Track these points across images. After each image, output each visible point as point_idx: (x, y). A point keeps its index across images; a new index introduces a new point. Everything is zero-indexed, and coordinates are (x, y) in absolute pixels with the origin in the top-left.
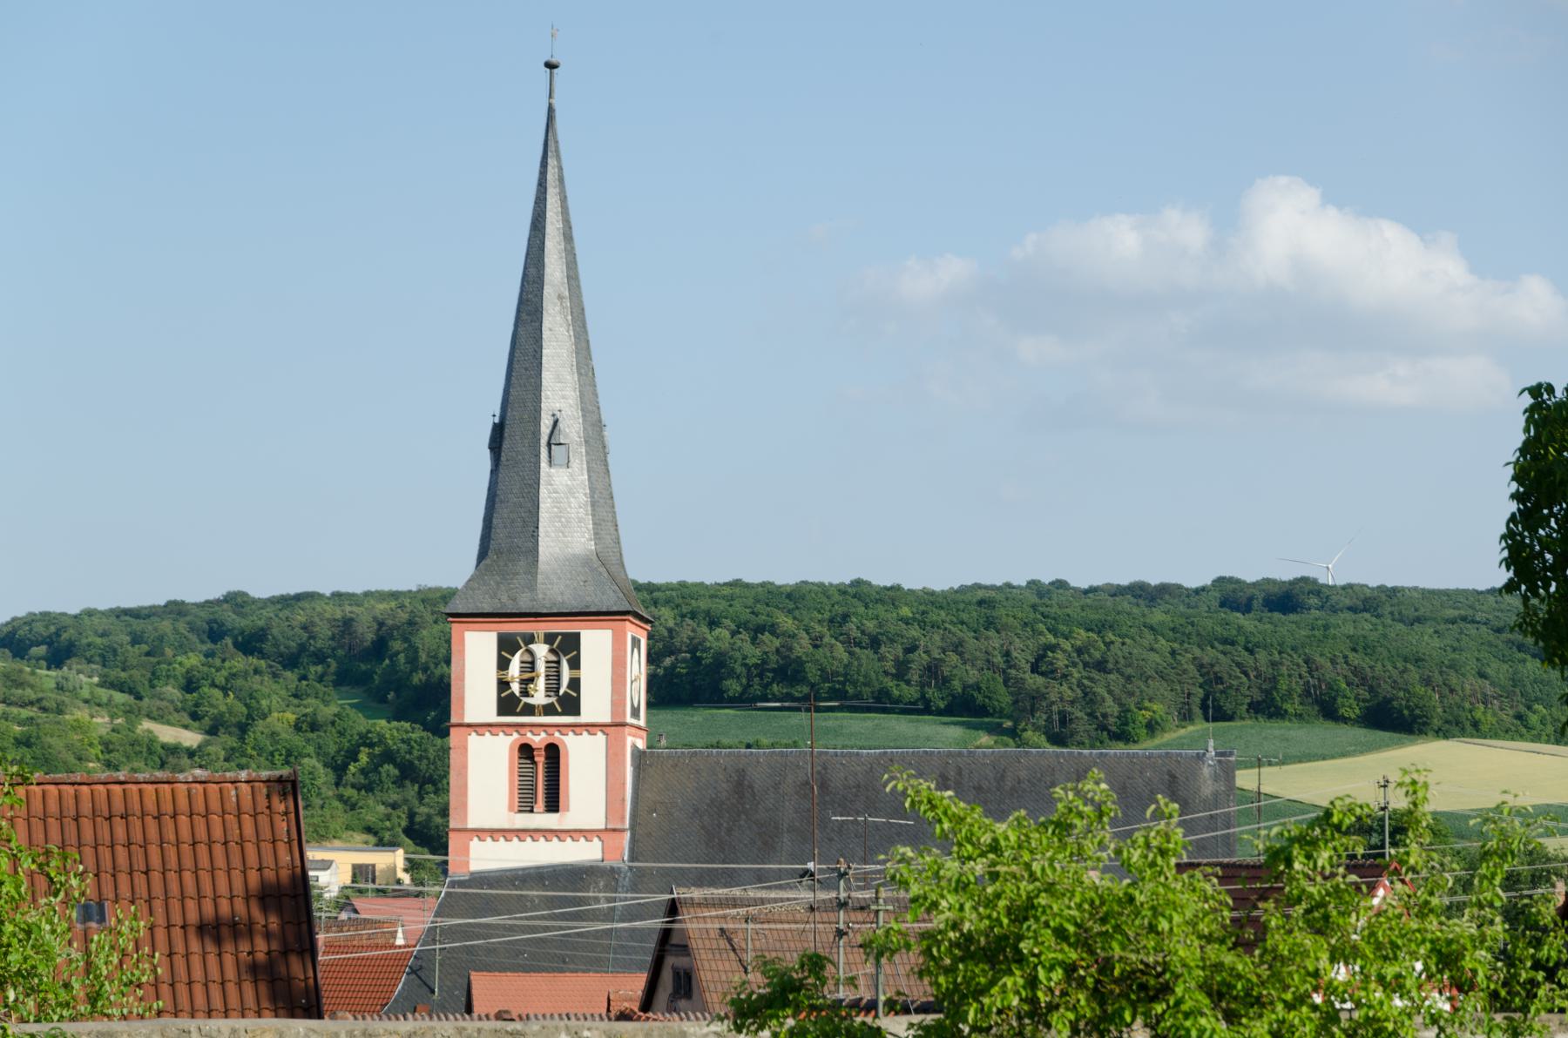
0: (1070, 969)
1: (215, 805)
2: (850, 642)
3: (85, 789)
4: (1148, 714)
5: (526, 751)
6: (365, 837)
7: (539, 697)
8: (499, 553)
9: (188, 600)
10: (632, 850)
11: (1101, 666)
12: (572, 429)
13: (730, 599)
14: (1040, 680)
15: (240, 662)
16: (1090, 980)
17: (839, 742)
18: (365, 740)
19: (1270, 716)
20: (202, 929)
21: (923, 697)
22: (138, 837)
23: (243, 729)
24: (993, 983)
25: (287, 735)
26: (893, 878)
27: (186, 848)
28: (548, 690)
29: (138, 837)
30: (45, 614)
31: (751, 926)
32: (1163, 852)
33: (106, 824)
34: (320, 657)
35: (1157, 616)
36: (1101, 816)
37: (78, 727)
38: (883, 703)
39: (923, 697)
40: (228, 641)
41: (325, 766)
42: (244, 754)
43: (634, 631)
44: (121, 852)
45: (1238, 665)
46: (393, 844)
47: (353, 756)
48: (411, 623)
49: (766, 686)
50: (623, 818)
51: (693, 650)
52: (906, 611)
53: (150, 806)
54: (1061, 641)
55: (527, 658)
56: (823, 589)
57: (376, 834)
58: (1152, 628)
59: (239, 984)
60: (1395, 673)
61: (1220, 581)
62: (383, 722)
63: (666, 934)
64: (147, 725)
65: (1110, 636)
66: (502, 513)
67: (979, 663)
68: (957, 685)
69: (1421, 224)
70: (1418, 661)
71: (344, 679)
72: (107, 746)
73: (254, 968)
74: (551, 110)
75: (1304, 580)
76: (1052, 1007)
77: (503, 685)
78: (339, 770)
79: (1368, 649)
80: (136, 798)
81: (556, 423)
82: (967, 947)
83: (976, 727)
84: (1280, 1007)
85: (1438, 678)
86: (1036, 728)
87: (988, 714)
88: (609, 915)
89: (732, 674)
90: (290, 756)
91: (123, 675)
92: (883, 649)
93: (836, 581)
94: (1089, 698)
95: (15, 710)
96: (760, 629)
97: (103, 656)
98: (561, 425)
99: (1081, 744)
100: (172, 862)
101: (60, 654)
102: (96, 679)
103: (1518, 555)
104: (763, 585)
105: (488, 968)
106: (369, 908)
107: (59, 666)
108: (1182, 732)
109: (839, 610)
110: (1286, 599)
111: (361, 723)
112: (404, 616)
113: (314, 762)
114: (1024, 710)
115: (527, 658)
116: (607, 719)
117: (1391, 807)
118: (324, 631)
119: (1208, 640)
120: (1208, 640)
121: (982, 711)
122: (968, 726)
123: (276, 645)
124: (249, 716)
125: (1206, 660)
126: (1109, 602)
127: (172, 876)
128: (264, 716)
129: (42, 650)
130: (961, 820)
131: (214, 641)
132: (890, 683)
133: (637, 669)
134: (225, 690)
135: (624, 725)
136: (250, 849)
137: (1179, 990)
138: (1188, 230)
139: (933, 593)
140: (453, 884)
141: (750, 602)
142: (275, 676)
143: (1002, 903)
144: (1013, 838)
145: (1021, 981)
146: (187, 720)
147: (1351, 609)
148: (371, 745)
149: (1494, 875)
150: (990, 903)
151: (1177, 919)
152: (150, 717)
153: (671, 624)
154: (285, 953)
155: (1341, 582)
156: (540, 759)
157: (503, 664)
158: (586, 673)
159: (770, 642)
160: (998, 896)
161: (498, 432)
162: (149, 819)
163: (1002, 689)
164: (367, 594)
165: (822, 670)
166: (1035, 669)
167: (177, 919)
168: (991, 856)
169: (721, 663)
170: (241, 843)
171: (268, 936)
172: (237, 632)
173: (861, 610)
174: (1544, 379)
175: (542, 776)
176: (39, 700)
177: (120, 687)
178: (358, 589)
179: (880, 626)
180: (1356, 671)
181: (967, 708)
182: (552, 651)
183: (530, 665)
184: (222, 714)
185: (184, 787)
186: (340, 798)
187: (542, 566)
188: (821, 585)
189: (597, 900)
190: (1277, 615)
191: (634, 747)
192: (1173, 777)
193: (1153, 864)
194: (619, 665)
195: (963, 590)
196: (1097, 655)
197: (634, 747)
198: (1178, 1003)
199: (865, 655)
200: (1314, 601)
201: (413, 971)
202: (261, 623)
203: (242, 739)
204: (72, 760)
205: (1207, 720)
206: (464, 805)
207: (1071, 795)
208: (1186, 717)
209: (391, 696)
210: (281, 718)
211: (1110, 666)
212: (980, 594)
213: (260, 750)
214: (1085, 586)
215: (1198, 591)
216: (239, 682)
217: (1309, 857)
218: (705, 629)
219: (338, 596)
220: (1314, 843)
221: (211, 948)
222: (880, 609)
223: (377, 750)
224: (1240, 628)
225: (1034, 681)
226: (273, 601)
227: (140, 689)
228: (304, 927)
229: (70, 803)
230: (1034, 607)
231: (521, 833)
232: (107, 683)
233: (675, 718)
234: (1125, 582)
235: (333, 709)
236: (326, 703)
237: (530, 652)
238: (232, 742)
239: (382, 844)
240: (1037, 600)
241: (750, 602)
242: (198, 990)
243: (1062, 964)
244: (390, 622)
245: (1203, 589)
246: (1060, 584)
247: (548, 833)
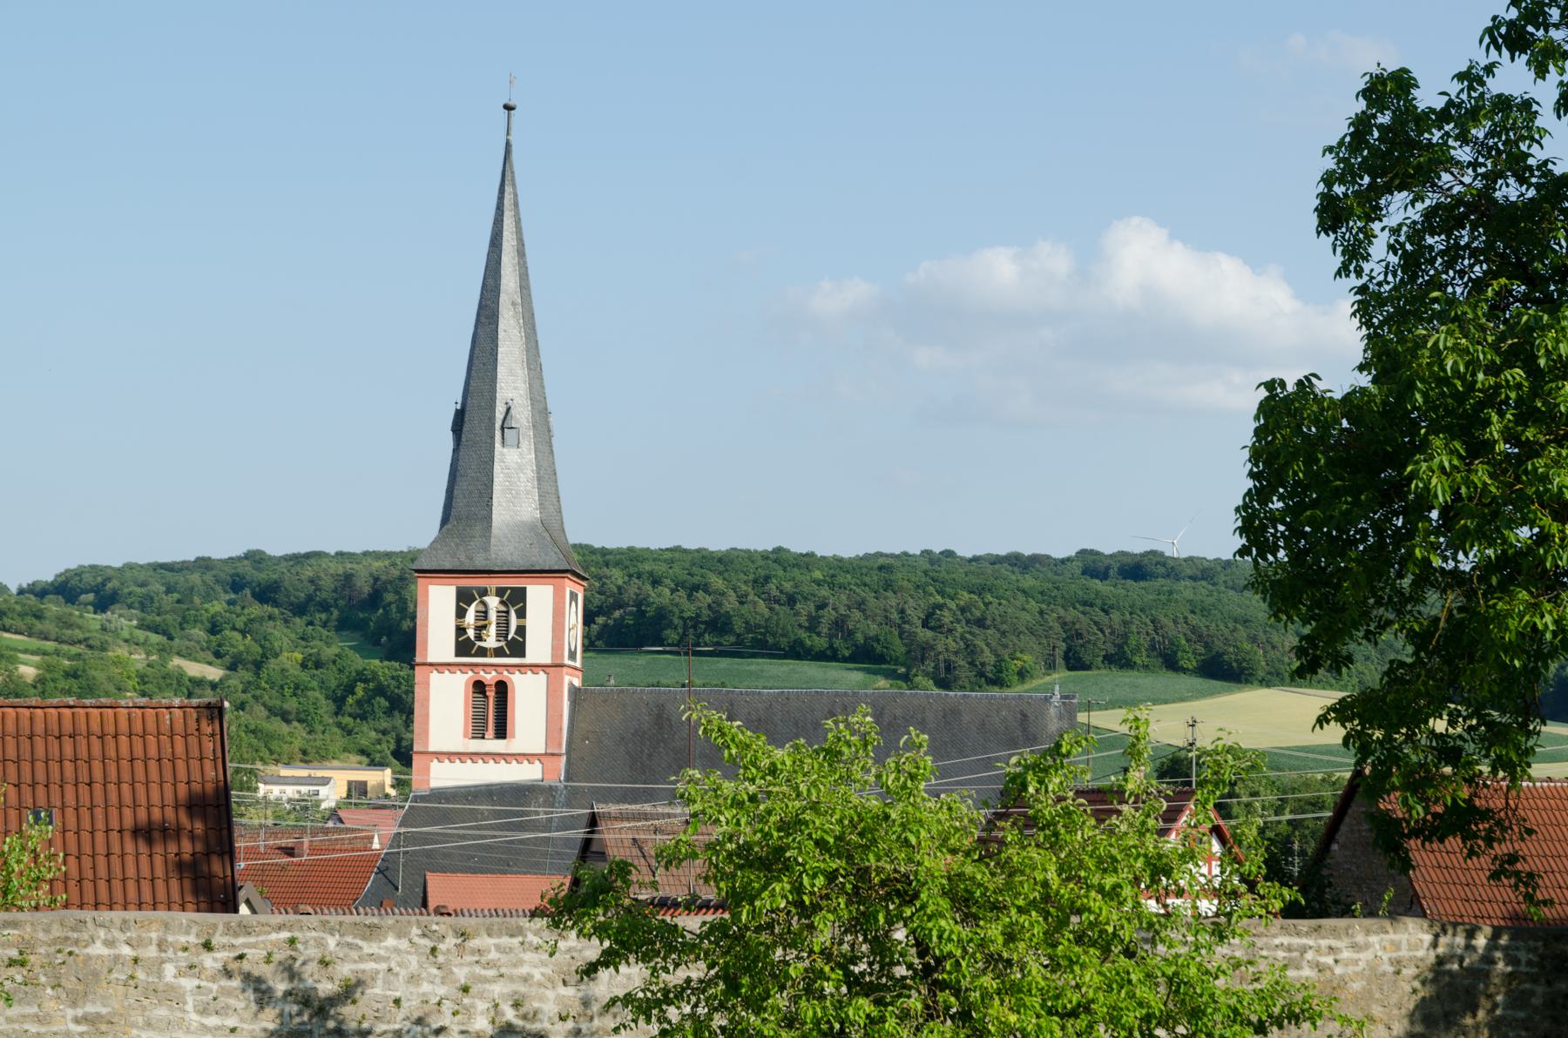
0: (831, 876)
1: (151, 727)
2: (771, 600)
3: (39, 711)
4: (1019, 663)
5: (479, 687)
6: (359, 758)
7: (491, 641)
8: (459, 519)
9: (215, 556)
10: (567, 772)
11: (981, 623)
12: (523, 415)
13: (670, 562)
14: (929, 634)
15: (256, 610)
16: (849, 886)
17: (760, 684)
18: (361, 677)
19: (1121, 667)
20: (136, 832)
21: (831, 646)
22: (83, 754)
23: (258, 665)
24: (764, 888)
25: (295, 672)
26: (682, 796)
27: (125, 764)
28: (498, 635)
29: (83, 754)
30: (93, 567)
31: (659, 837)
32: (912, 777)
33: (56, 742)
34: (325, 607)
35: (1028, 582)
36: (866, 746)
37: (118, 662)
38: (797, 652)
39: (831, 646)
40: (247, 591)
41: (327, 698)
42: (258, 687)
43: (570, 586)
44: (68, 766)
45: (1096, 623)
46: (381, 765)
47: (350, 689)
48: (402, 579)
49: (701, 635)
50: (560, 745)
51: (639, 604)
52: (818, 575)
53: (95, 728)
54: (948, 601)
55: (481, 608)
56: (750, 555)
57: (368, 755)
58: (1024, 592)
59: (167, 881)
60: (1227, 632)
61: (1083, 552)
62: (377, 662)
63: (587, 843)
64: (176, 661)
65: (989, 598)
66: (462, 485)
67: (879, 619)
68: (859, 637)
69: (1256, 262)
70: (1246, 622)
71: (344, 625)
72: (143, 678)
73: (180, 866)
74: (508, 145)
75: (1153, 553)
76: (816, 908)
77: (461, 630)
78: (339, 702)
79: (1205, 611)
80: (83, 720)
81: (508, 410)
82: (745, 857)
83: (875, 673)
84: (1013, 911)
85: (1262, 637)
86: (926, 674)
87: (886, 662)
88: (547, 826)
89: (671, 625)
90: (299, 690)
91: (158, 619)
92: (798, 606)
93: (760, 549)
94: (970, 650)
95: (65, 647)
96: (695, 588)
97: (141, 603)
98: (512, 412)
99: (963, 688)
100: (113, 776)
101: (104, 602)
102: (135, 622)
103: (1252, 525)
104: (698, 551)
105: (443, 870)
106: (352, 818)
107: (104, 611)
108: (1048, 679)
109: (763, 573)
110: (1136, 569)
111: (357, 662)
112: (396, 573)
113: (317, 694)
114: (915, 659)
115: (481, 608)
116: (548, 661)
117: (1198, 744)
118: (327, 583)
119: (1070, 603)
120: (1070, 603)
121: (881, 659)
122: (868, 671)
123: (288, 596)
124: (264, 655)
125: (1069, 619)
126: (989, 569)
127: (112, 788)
128: (276, 655)
129: (91, 597)
130: (748, 746)
131: (236, 592)
132: (803, 635)
133: (574, 618)
134: (243, 633)
135: (562, 666)
136: (181, 765)
137: (924, 896)
138: (1057, 260)
139: (841, 560)
140: (415, 799)
141: (687, 565)
142: (286, 621)
143: (773, 819)
144: (788, 763)
145: (788, 887)
146: (211, 658)
147: (1193, 578)
148: (366, 681)
149: (1207, 801)
150: (762, 819)
151: (923, 833)
152: (179, 654)
153: (620, 582)
154: (207, 855)
155: (1184, 555)
156: (491, 694)
157: (461, 613)
158: (530, 622)
160: (769, 812)
161: (460, 418)
162: (93, 738)
163: (897, 641)
164: (366, 554)
165: (747, 623)
166: (925, 624)
167: (115, 824)
168: (769, 778)
169: (662, 616)
170: (173, 760)
171: (193, 838)
172: (259, 585)
173: (780, 573)
174: (1277, 375)
175: (492, 706)
176: (86, 639)
177: (155, 629)
178: (357, 549)
179: (796, 586)
180: (1194, 630)
181: (867, 656)
182: (502, 602)
183: (483, 614)
184: (241, 653)
185: (125, 711)
186: (339, 725)
187: (495, 531)
188: (748, 551)
189: (537, 813)
190: (1130, 582)
191: (571, 684)
192: (1025, 715)
193: (904, 787)
194: (558, 614)
195: (867, 557)
196: (978, 614)
197: (571, 684)
198: (923, 907)
199: (782, 610)
200: (1161, 570)
201: (380, 871)
202: (275, 577)
203: (257, 675)
204: (112, 689)
205: (1070, 669)
206: (426, 731)
207: (842, 726)
208: (1051, 666)
209: (384, 639)
210: (290, 659)
211: (988, 622)
212: (881, 561)
213: (272, 684)
214: (969, 555)
215: (1063, 561)
216: (256, 626)
217: (1041, 782)
218: (649, 587)
219: (340, 554)
220: (1046, 770)
221: (143, 848)
222: (796, 572)
223: (371, 685)
224: (1097, 593)
225: (925, 635)
226: (287, 558)
227: (172, 631)
228: (225, 832)
229: (25, 724)
230: (926, 573)
231: (474, 756)
232: (143, 626)
233: (619, 666)
234: (1003, 552)
235: (334, 650)
236: (328, 645)
237: (484, 604)
238: (248, 676)
239: (374, 764)
240: (928, 566)
241: (687, 565)
242: (131, 885)
243: (824, 872)
244: (384, 578)
245: (1069, 559)
246: (949, 554)
247: (506, 757)
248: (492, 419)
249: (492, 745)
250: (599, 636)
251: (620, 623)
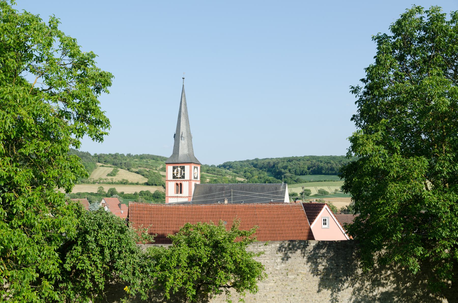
5: (177, 184)
7: (179, 176)
25: (257, 180)
34: (265, 168)
71: (268, 171)
74: (183, 85)
77: (174, 174)
89: (323, 170)
112: (277, 161)
118: (266, 164)
152: (238, 177)
156: (179, 185)
157: (174, 171)
158: (185, 172)
159: (329, 165)
169: (322, 168)
175: (179, 188)
177: (235, 172)
183: (178, 171)
248: (179, 135)
249: (179, 195)
250: (311, 172)
251: (314, 170)
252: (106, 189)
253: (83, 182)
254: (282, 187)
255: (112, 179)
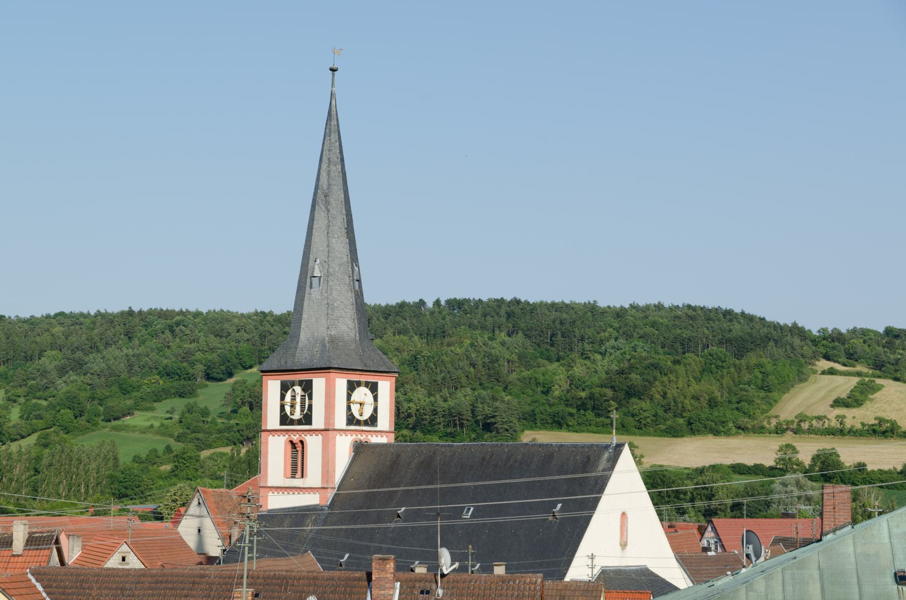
74: (332, 94)
77: (282, 407)
116: (322, 427)
156: (299, 449)
157: (283, 397)
182: (303, 390)
183: (294, 397)
192: (588, 458)
252: (807, 451)
253: (742, 429)
254: (606, 455)
255: (841, 419)
